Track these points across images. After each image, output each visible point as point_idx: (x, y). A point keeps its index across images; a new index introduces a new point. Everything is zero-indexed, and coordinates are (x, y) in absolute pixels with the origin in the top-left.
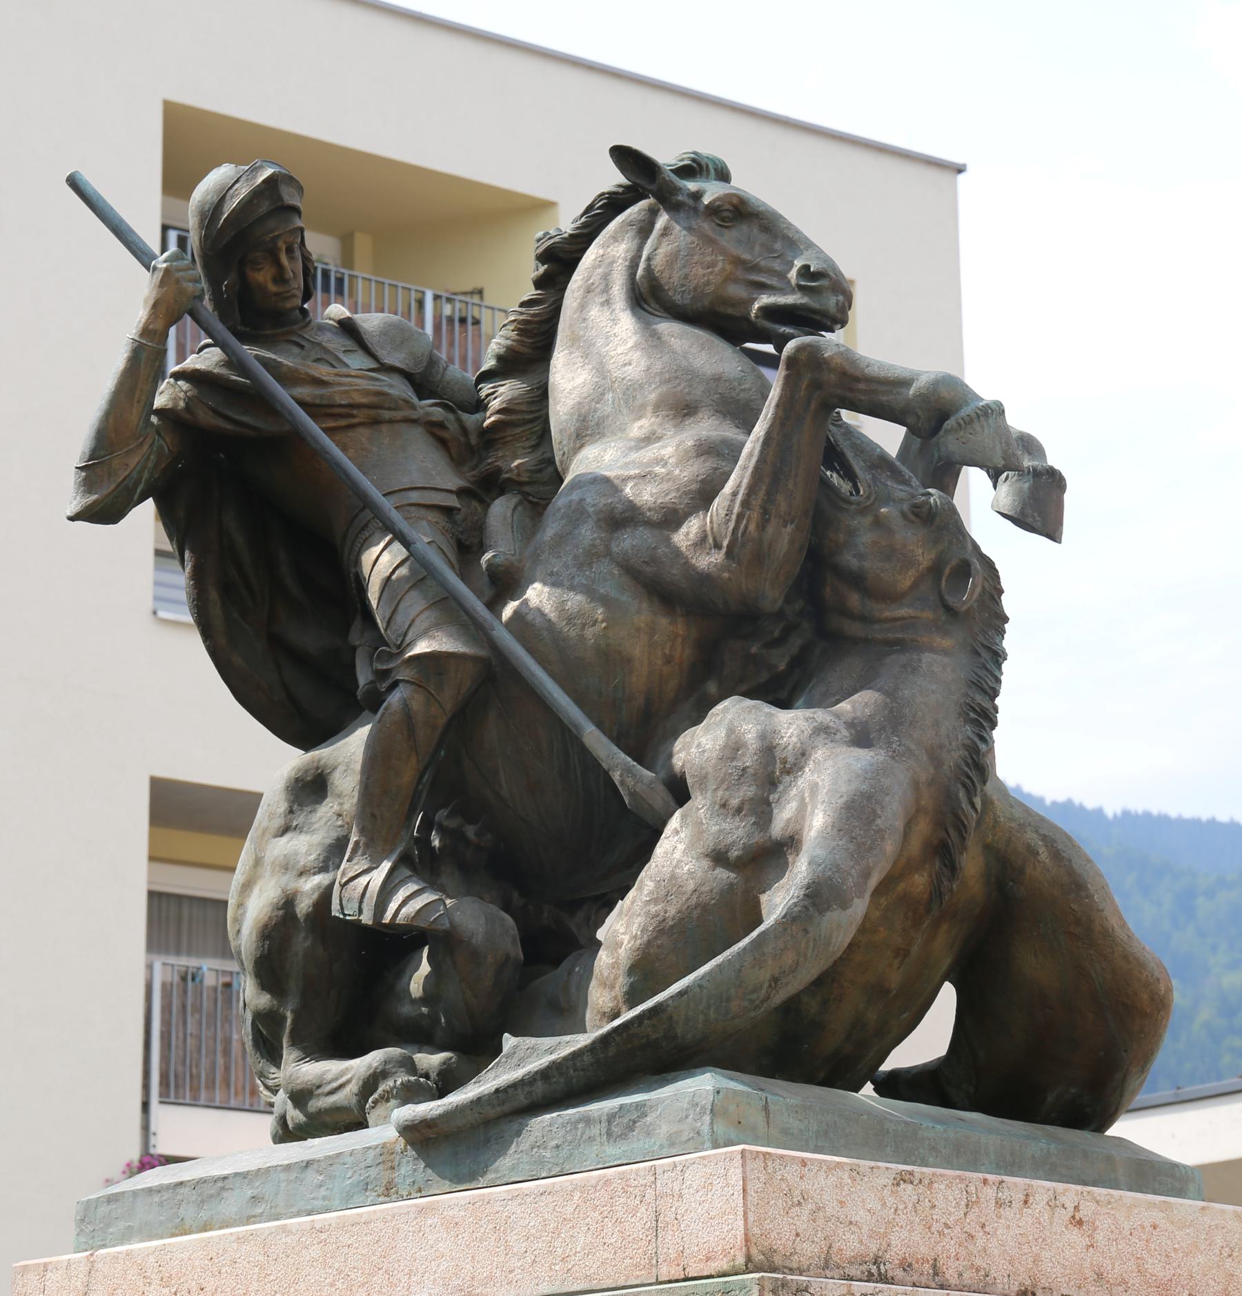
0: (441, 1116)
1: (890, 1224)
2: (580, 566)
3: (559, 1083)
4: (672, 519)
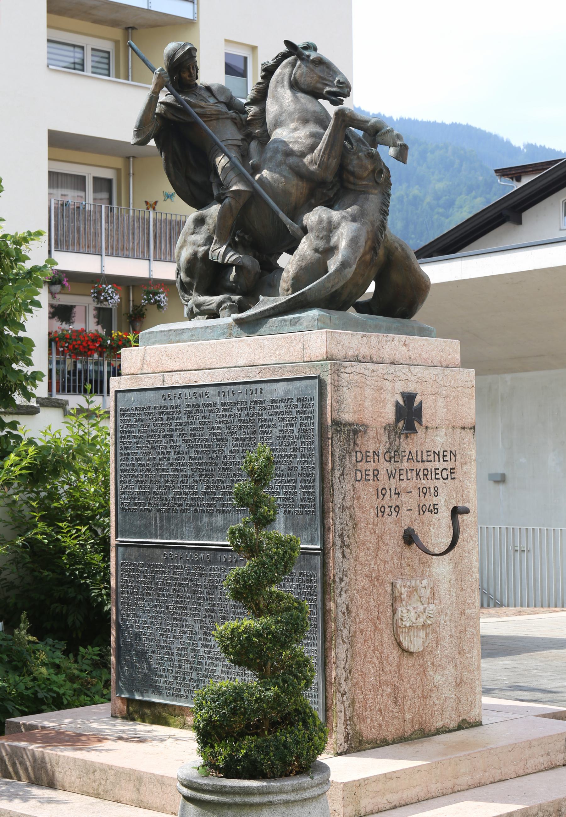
0: (245, 318)
1: (360, 347)
2: (277, 166)
3: (277, 310)
4: (303, 155)
